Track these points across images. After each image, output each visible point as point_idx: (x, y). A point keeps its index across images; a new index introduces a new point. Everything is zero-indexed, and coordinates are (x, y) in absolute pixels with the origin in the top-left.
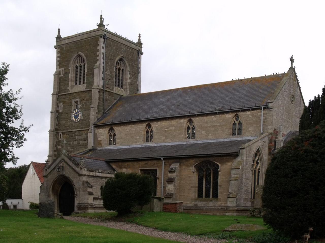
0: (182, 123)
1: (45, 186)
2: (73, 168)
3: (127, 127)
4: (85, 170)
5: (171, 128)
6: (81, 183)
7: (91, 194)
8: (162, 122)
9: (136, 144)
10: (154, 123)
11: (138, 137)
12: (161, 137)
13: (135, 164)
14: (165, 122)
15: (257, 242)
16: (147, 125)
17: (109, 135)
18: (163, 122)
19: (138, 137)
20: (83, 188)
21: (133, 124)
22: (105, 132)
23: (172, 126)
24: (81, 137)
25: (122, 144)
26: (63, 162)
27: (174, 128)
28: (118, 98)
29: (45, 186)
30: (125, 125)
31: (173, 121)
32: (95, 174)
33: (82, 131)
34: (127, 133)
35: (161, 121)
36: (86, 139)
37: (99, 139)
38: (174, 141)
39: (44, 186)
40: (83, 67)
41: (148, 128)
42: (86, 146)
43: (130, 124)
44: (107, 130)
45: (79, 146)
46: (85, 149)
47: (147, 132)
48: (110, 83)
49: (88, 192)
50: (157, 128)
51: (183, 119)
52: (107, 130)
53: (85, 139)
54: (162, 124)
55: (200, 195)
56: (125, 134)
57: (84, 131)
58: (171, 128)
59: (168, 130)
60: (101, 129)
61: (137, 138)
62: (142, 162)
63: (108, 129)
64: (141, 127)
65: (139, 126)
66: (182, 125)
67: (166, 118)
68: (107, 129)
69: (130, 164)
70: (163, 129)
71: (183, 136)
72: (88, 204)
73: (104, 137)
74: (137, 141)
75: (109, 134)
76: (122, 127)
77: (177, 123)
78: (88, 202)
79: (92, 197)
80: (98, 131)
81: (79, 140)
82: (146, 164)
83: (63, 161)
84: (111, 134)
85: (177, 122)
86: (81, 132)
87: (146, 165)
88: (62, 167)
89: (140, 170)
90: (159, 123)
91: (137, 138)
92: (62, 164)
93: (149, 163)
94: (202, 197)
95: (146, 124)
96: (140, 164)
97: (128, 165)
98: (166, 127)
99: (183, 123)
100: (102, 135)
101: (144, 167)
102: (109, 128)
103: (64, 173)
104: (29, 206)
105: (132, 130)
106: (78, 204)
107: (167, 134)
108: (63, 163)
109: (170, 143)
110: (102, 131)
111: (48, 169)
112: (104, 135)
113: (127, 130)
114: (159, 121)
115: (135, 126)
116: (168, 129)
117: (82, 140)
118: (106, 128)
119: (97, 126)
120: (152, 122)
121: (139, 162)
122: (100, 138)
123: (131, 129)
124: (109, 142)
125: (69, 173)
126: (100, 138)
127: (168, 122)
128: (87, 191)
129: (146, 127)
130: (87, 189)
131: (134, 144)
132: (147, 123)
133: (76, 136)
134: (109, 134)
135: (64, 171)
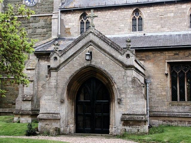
0: (184, 9)
1: (53, 84)
2: (112, 56)
3: (107, 13)
5: (169, 15)
8: (155, 8)
9: (119, 33)
10: (144, 8)
11: (123, 25)
12: (156, 25)
13: (158, 54)
14: (160, 7)
15: (161, 142)
16: (134, 11)
17: (80, 22)
18: (157, 7)
19: (123, 25)
20: (133, 87)
22: (75, 19)
23: (171, 13)
24: (36, 25)
26: (91, 45)
27: (172, 15)
29: (53, 84)
31: (171, 7)
33: (40, 17)
34: (106, 20)
35: (154, 6)
36: (49, 26)
37: (67, 27)
38: (173, 30)
39: (51, 84)
41: (134, 14)
42: (45, 35)
43: (110, 10)
44: (77, 16)
45: (35, 35)
46: (44, 40)
47: (134, 19)
50: (148, 15)
51: (186, 4)
52: (77, 16)
53: (43, 27)
54: (155, 10)
55: (174, 98)
56: (104, 21)
57: (42, 18)
58: (169, 15)
59: (165, 18)
61: (121, 26)
62: (170, 52)
63: (80, 15)
64: (126, 13)
65: (124, 12)
66: (185, 11)
67: (163, 2)
68: (78, 15)
69: (151, 54)
70: (158, 16)
71: (185, 24)
73: (74, 24)
74: (120, 30)
75: (80, 21)
76: (100, 13)
77: (176, 9)
80: (65, 16)
81: (36, 28)
82: (175, 54)
83: (90, 43)
84: (82, 20)
85: (177, 7)
86: (38, 19)
87: (177, 56)
89: (167, 62)
90: (152, 8)
91: (121, 26)
92: (88, 49)
93: (181, 54)
94: (176, 100)
95: (133, 10)
96: (166, 55)
97: (146, 55)
98: (161, 14)
99: (186, 9)
100: (70, 22)
101: (173, 59)
102: (81, 14)
105: (113, 16)
106: (123, 115)
107: (162, 22)
108: (91, 47)
109: (167, 32)
110: (70, 17)
111: (60, 57)
112: (73, 22)
113: (106, 16)
114: (151, 6)
115: (118, 12)
116: (165, 16)
117: (39, 28)
118: (76, 13)
119: (65, 12)
120: (142, 7)
121: (164, 53)
122: (68, 25)
123: (112, 15)
124: (80, 31)
125: (103, 63)
126: (68, 25)
127: (164, 7)
129: (133, 14)
131: (117, 33)
132: (134, 9)
133: (30, 23)
134: (80, 21)
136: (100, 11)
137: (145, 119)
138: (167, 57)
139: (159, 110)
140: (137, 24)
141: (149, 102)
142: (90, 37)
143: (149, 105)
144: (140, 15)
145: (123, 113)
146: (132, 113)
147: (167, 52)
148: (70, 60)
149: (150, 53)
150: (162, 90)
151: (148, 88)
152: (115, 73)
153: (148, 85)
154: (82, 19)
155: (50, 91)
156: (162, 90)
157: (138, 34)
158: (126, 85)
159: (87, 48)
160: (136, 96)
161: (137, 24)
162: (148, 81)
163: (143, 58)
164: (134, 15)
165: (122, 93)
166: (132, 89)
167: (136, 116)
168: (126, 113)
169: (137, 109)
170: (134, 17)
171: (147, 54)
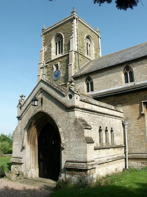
4: (77, 98)
6: (72, 121)
7: (90, 141)
10: (133, 64)
11: (117, 80)
16: (125, 68)
18: (144, 61)
20: (75, 130)
21: (110, 70)
25: (100, 89)
28: (88, 62)
30: (101, 72)
32: (92, 107)
35: (140, 61)
40: (61, 42)
43: (106, 70)
48: (82, 49)
49: (86, 137)
60: (78, 80)
63: (85, 79)
72: (86, 162)
78: (86, 159)
79: (91, 147)
88: (40, 100)
89: (143, 102)
95: (124, 67)
103: (43, 109)
104: (92, 137)
114: (138, 61)
120: (130, 63)
121: (140, 94)
128: (83, 135)
129: (124, 70)
130: (83, 132)
132: (125, 66)
135: (43, 105)
136: (99, 73)
137: (86, 168)
138: (143, 97)
139: (137, 152)
140: (130, 77)
141: (128, 143)
142: (41, 84)
143: (128, 146)
144: (130, 69)
145: (67, 159)
146: (74, 160)
147: (142, 93)
148: (28, 108)
149: (127, 96)
150: (140, 131)
151: (126, 130)
152: (60, 116)
153: (126, 127)
154: (88, 81)
155: (18, 137)
156: (140, 131)
157: (130, 84)
158: (70, 128)
159: (39, 95)
160: (78, 139)
161: (130, 77)
162: (126, 123)
163: (121, 102)
164: (126, 71)
165: (66, 136)
166: (75, 133)
167: (78, 164)
168: (70, 159)
169: (80, 155)
170: (126, 72)
171: (124, 97)
